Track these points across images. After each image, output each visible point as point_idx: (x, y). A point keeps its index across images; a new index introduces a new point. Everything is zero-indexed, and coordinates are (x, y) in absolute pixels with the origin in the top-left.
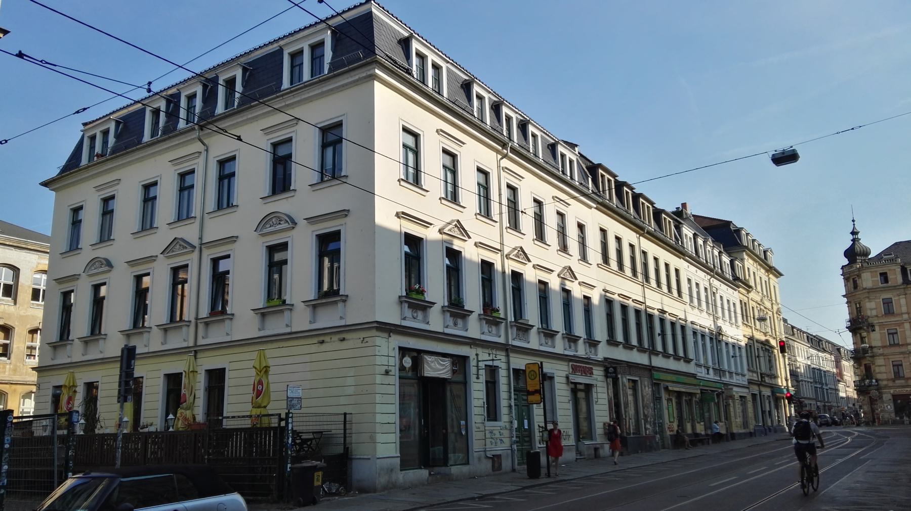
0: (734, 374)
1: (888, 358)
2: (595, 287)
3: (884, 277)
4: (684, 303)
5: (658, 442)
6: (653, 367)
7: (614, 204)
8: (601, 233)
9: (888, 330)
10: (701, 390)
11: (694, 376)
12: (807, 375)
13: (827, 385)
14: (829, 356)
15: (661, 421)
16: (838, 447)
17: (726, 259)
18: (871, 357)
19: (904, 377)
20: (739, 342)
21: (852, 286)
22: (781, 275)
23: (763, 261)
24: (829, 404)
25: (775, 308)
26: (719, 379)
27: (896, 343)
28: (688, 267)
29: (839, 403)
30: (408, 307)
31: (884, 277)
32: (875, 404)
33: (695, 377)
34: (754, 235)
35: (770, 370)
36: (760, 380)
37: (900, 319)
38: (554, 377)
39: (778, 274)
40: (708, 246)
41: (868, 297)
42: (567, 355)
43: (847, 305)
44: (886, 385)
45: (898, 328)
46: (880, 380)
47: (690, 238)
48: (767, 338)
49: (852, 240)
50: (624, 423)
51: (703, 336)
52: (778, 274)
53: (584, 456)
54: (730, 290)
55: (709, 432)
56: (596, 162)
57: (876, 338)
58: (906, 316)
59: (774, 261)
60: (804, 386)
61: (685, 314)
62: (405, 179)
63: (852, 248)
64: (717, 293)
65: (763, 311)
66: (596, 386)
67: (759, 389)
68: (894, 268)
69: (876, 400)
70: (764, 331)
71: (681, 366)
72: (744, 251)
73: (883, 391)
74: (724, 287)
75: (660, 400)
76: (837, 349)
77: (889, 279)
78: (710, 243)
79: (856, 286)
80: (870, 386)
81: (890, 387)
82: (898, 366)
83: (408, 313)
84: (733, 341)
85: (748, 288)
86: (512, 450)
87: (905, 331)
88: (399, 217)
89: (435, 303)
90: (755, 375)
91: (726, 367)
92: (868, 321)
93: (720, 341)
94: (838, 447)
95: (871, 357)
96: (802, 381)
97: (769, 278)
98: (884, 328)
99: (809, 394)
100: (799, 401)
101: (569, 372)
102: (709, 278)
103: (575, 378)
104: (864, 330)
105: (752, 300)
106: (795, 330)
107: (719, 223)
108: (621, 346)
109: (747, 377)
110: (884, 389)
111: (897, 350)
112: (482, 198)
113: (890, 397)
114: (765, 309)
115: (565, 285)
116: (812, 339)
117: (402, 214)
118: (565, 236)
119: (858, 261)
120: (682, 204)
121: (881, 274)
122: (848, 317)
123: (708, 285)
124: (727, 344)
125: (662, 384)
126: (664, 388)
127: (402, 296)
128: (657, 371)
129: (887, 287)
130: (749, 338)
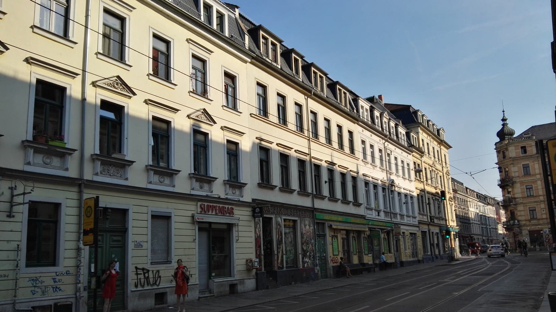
0: (405, 216)
1: (526, 206)
2: (244, 134)
3: (524, 149)
4: (357, 159)
5: (317, 274)
6: (315, 209)
7: (347, 108)
8: (298, 108)
9: (526, 186)
10: (369, 228)
11: (363, 217)
12: (476, 219)
13: (490, 226)
14: (492, 207)
15: (325, 255)
16: (474, 273)
17: (402, 130)
18: (514, 205)
19: (537, 218)
21: (502, 156)
22: (451, 147)
23: (437, 136)
24: (492, 238)
25: (445, 170)
26: (390, 220)
27: (531, 195)
29: (498, 237)
30: (196, 181)
31: (524, 149)
33: (364, 218)
34: (428, 117)
35: (439, 214)
36: (429, 221)
37: (535, 178)
38: (171, 216)
39: (448, 147)
40: (384, 118)
41: (513, 164)
42: (193, 195)
43: (498, 170)
44: (524, 224)
45: (533, 184)
46: (520, 221)
47: (404, 135)
48: (437, 191)
49: (502, 125)
50: (276, 258)
51: (375, 186)
52: (448, 147)
53: (214, 294)
54: (405, 154)
55: (377, 262)
56: (335, 80)
57: (518, 191)
58: (538, 176)
59: (445, 137)
60: (474, 227)
61: (332, 157)
62: (226, 106)
63: (502, 130)
64: (391, 154)
65: (435, 171)
66: (238, 225)
67: (429, 228)
68: (531, 143)
69: (518, 235)
70: (434, 186)
71: (351, 209)
72: (419, 126)
73: (523, 228)
74: (398, 150)
75: (324, 237)
76: (497, 203)
77: (527, 151)
78: (386, 114)
79: (504, 157)
80: (514, 225)
81: (527, 226)
82: (533, 210)
83: (197, 185)
84: (405, 191)
85: (421, 153)
86: (76, 297)
87: (537, 186)
88: (147, 104)
89: (247, 184)
90: (425, 217)
91: (398, 210)
92: (512, 180)
93: (392, 191)
94: (474, 273)
95: (514, 205)
96: (473, 223)
97: (441, 149)
98: (523, 184)
99: (478, 232)
100: (470, 236)
101: (197, 212)
102: (384, 142)
103: (204, 218)
104: (510, 186)
105: (424, 162)
106: (468, 190)
107: (402, 107)
108: (351, 204)
109: (417, 219)
110: (523, 227)
111: (533, 200)
112: (281, 120)
113: (527, 232)
114: (436, 171)
115: (200, 127)
116: (480, 196)
117: (225, 128)
118: (330, 141)
119: (506, 139)
120: (379, 96)
121: (522, 147)
122: (499, 178)
123: (383, 148)
124: (399, 194)
125: (326, 223)
126: (329, 227)
127: (191, 174)
128: (321, 212)
129: (526, 156)
130: (420, 190)
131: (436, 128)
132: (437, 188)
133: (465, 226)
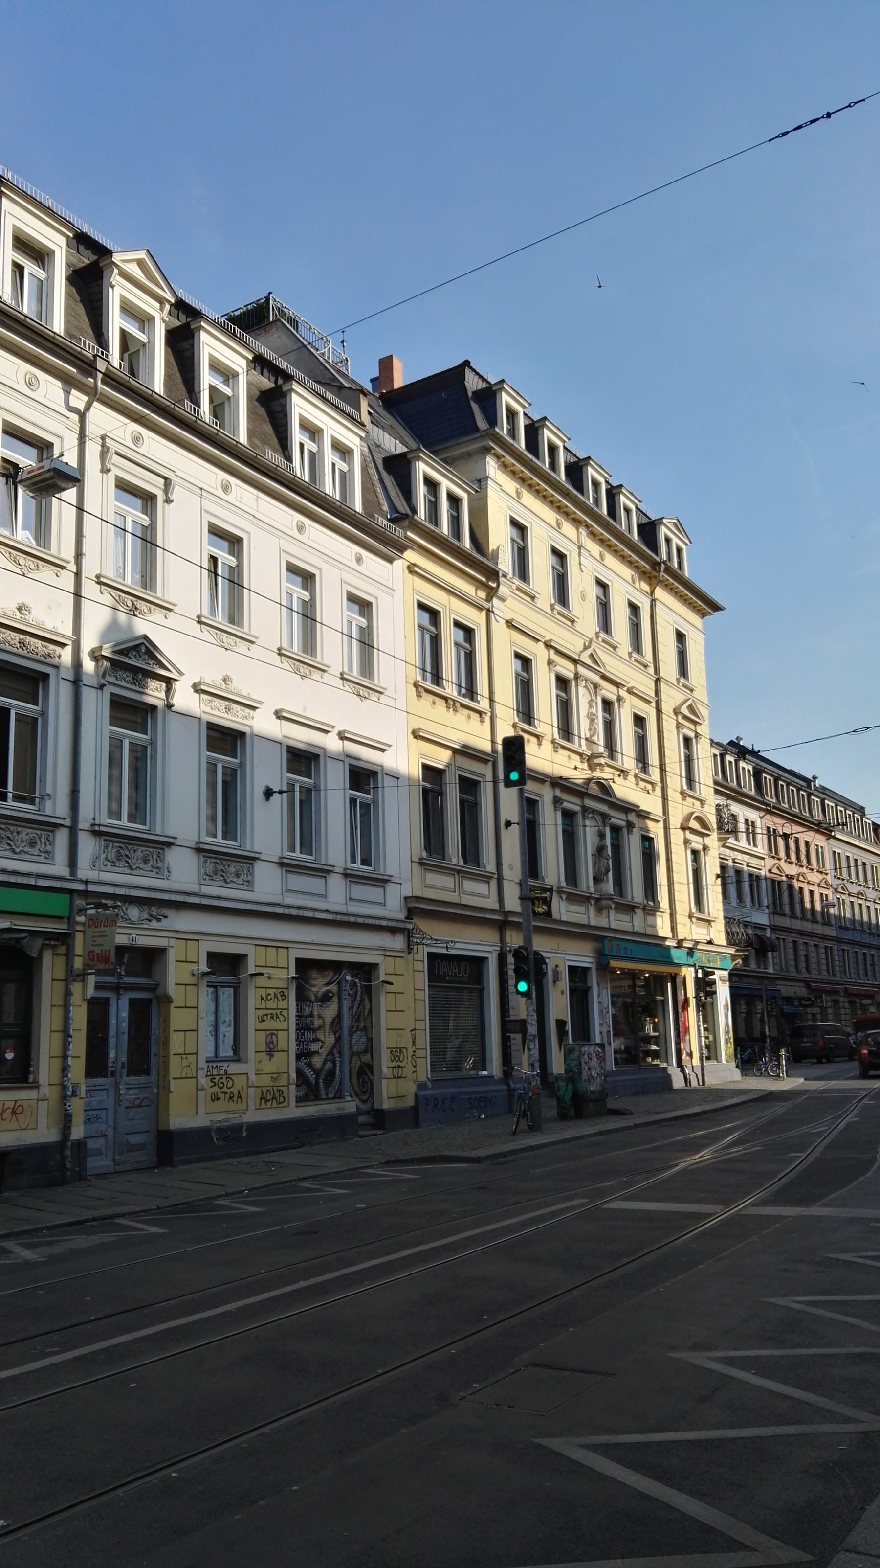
20: (725, 861)
28: (359, 560)
32: (734, 958)
72: (487, 450)
97: (653, 601)
118: (435, 672)
131: (633, 507)
132: (596, 761)
133: (860, 957)
